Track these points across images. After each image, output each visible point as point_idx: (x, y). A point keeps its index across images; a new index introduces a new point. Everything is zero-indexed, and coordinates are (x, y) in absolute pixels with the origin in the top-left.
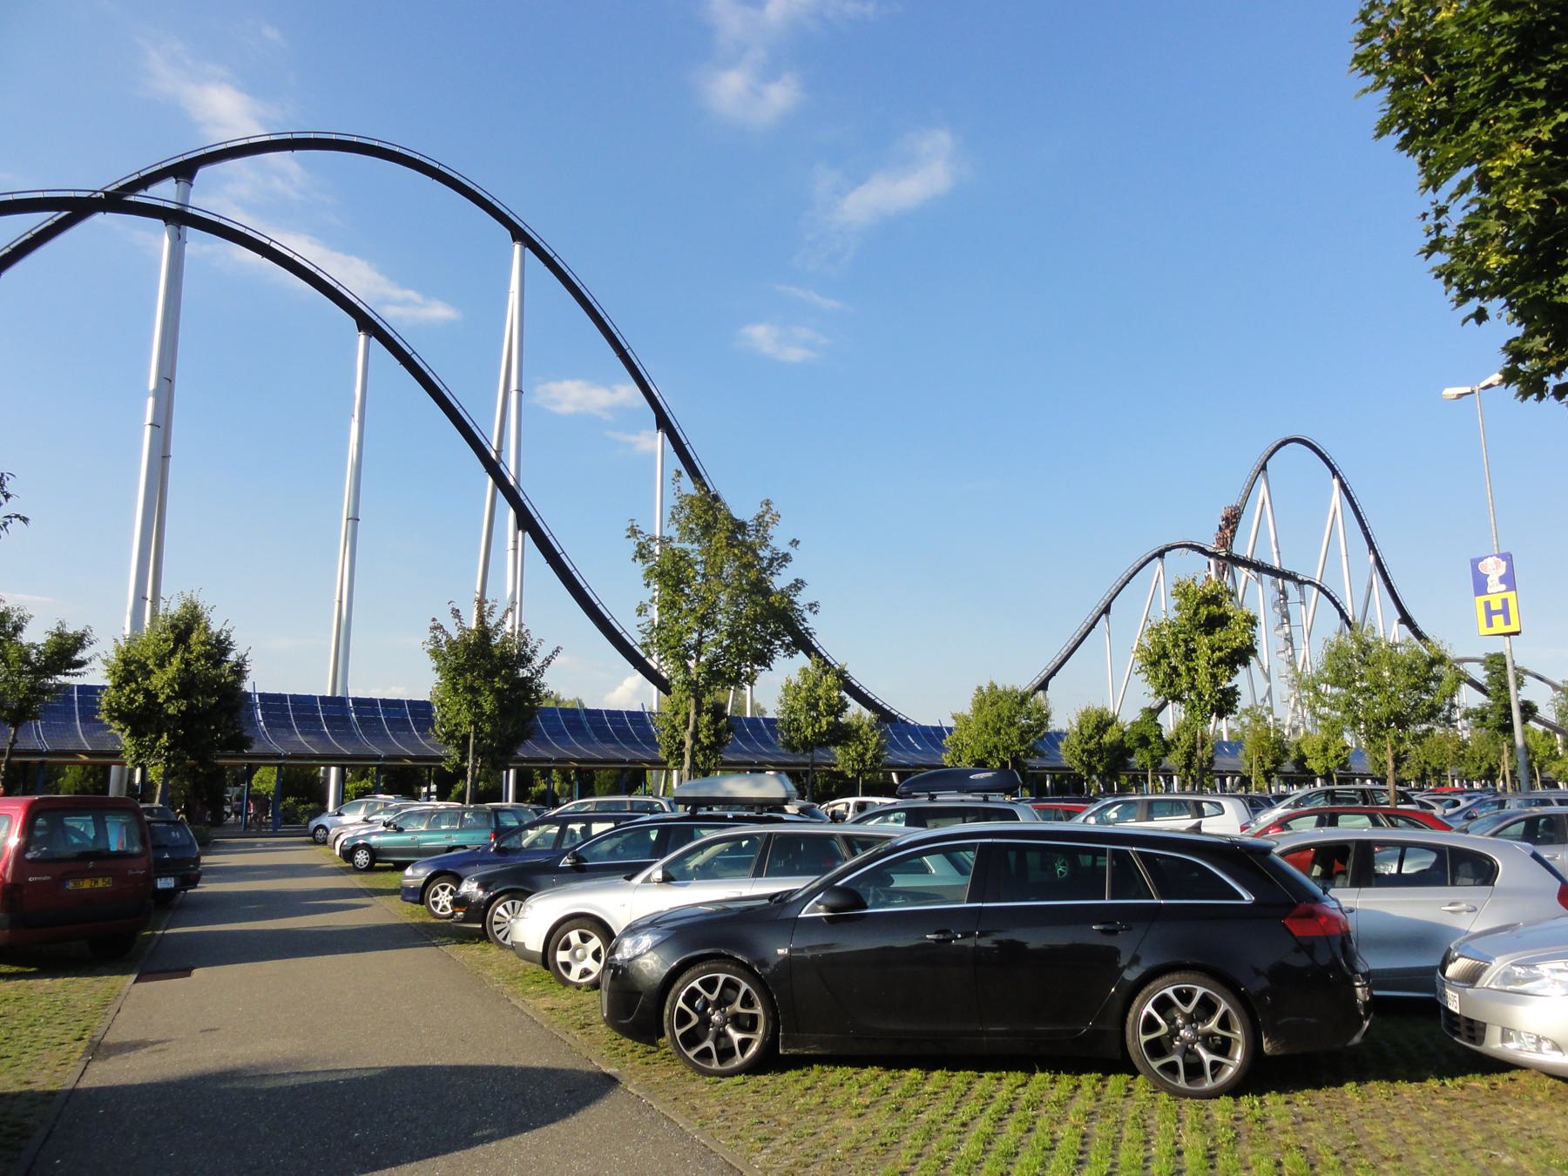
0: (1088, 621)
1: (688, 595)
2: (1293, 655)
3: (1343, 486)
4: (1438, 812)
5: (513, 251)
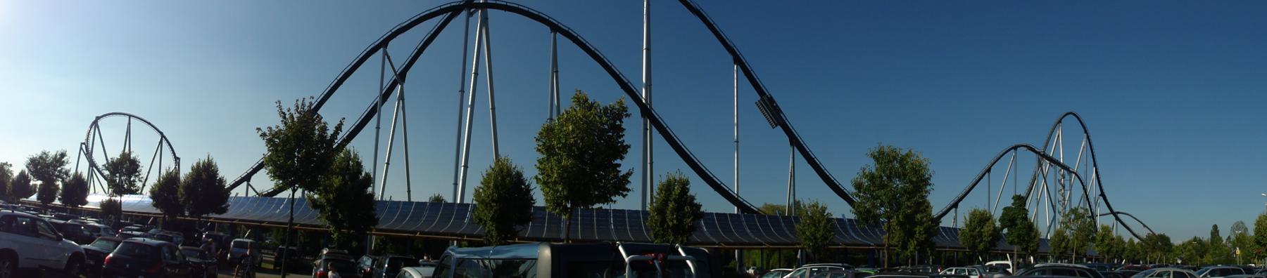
1: (830, 232)
3: (1088, 137)
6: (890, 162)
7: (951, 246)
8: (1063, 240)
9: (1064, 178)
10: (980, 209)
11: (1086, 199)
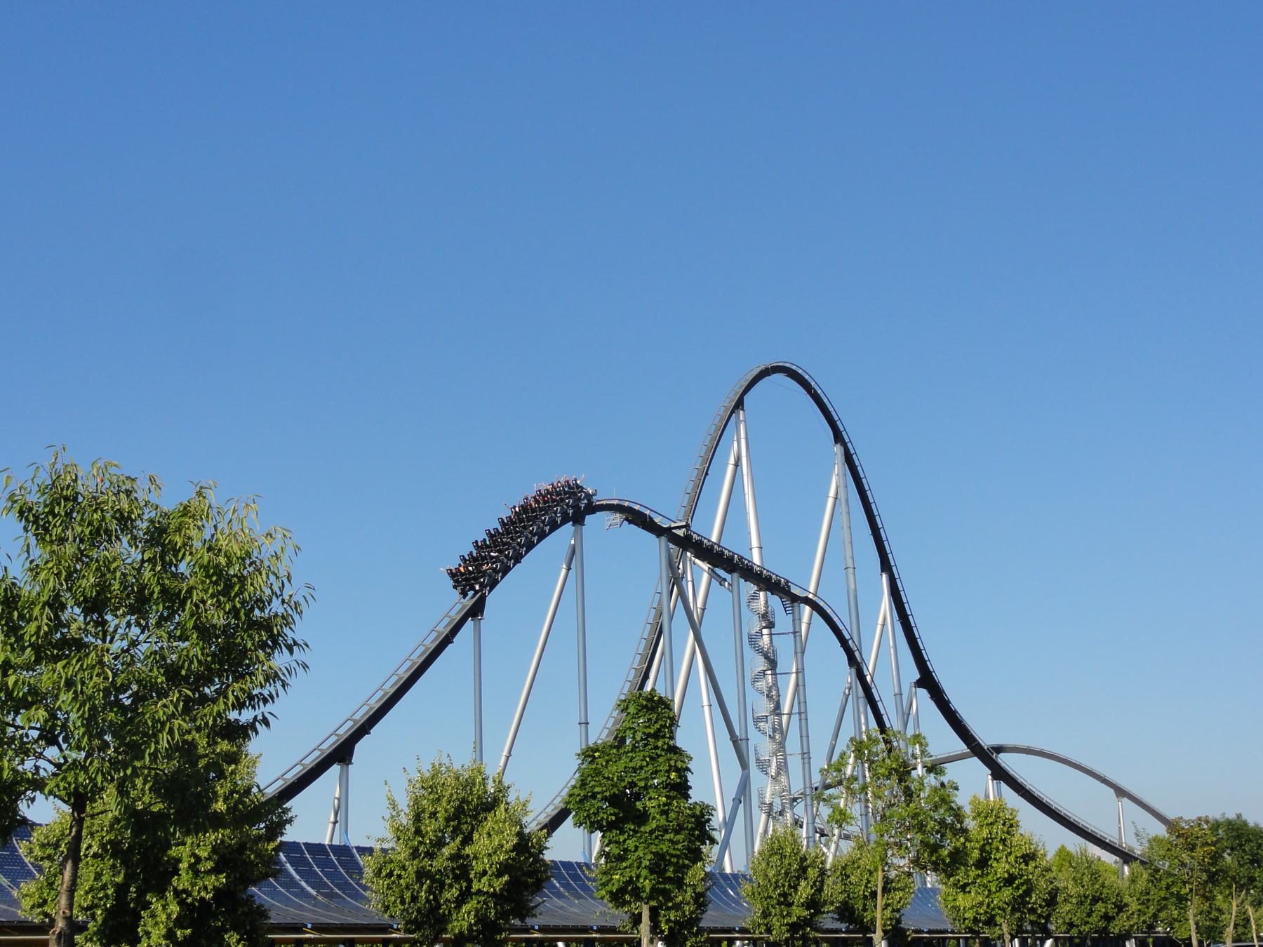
2: (775, 684)
3: (849, 459)
4: (615, 751)
6: (99, 534)
7: (932, 928)
8: (803, 870)
9: (771, 625)
10: (457, 766)
11: (862, 701)
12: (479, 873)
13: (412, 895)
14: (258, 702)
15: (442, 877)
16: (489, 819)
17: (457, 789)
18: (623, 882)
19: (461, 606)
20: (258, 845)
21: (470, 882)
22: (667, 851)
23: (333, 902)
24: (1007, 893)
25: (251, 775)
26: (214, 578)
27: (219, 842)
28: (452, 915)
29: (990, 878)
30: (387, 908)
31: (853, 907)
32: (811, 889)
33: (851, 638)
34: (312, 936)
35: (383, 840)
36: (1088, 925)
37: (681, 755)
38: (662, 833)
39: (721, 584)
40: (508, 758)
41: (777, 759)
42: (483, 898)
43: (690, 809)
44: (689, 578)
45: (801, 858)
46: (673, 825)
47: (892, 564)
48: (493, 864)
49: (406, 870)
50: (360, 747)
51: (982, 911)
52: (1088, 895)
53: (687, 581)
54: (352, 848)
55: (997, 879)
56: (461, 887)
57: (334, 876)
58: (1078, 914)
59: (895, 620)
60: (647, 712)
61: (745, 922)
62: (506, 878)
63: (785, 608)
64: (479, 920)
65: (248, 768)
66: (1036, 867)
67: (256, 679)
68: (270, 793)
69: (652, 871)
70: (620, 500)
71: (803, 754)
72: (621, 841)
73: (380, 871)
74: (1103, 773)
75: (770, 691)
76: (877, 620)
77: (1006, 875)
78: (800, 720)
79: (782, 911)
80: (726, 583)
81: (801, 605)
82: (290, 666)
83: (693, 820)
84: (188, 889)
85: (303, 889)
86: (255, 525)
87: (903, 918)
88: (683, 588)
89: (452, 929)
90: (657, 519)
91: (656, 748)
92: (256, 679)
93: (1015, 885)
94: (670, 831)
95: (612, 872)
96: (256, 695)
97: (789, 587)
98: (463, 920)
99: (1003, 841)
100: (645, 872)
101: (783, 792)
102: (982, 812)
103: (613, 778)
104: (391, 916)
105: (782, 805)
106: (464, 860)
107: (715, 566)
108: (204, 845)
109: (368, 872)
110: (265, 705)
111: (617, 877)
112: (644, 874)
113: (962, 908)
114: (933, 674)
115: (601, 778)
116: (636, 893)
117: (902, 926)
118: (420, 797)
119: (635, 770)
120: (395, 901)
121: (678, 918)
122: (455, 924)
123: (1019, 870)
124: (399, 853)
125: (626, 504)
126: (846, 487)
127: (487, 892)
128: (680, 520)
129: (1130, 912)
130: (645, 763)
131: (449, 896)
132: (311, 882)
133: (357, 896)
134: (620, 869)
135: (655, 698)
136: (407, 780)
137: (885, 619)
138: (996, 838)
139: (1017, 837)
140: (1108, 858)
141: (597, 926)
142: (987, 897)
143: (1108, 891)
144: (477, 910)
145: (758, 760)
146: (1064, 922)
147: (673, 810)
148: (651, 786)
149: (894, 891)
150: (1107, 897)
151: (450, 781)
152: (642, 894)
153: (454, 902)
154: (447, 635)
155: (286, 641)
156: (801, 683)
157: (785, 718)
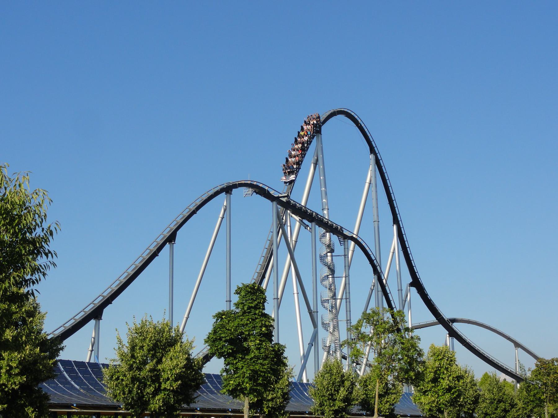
0: (151, 248)
2: (334, 282)
3: (378, 162)
5: (88, 353)
10: (155, 322)
11: (380, 293)
12: (165, 379)
13: (129, 390)
14: (30, 283)
15: (145, 381)
16: (172, 350)
17: (155, 334)
18: (235, 385)
19: (163, 236)
20: (44, 361)
21: (160, 384)
22: (259, 369)
23: (88, 393)
24: (448, 396)
25: (41, 323)
26: (4, 216)
27: (22, 358)
28: (150, 401)
29: (439, 388)
30: (116, 396)
31: (369, 402)
32: (346, 392)
33: (376, 259)
34: (76, 410)
35: (114, 360)
36: (495, 415)
37: (268, 318)
38: (256, 360)
39: (305, 228)
40: (187, 318)
41: (333, 323)
42: (167, 393)
43: (272, 347)
44: (289, 225)
45: (341, 376)
46: (263, 355)
47: (399, 220)
48: (173, 374)
49: (126, 377)
50: (106, 311)
51: (434, 405)
52: (496, 399)
53: (287, 226)
54: (100, 364)
55: (443, 389)
56: (156, 386)
57: (90, 379)
58: (490, 409)
59: (400, 250)
60: (251, 295)
61: (310, 409)
62: (180, 382)
63: (340, 242)
64: (164, 404)
65: (39, 320)
66: (463, 383)
67: (26, 271)
68: (56, 334)
69: (250, 380)
70: (252, 181)
71: (347, 320)
72: (235, 363)
73: (112, 377)
74: (508, 334)
75: (330, 286)
76: (390, 250)
77: (447, 387)
78: (346, 302)
79: (330, 403)
80: (309, 228)
81: (349, 240)
82: (46, 264)
83: (273, 353)
84: (5, 383)
85: (72, 385)
86: (28, 188)
87: (395, 408)
88: (285, 230)
89: (150, 408)
90: (272, 192)
91: (255, 314)
92: (26, 271)
93: (452, 392)
94: (261, 358)
95: (229, 380)
96: (28, 279)
97: (343, 231)
98: (156, 403)
99: (447, 369)
100: (246, 380)
101: (336, 341)
102: (436, 353)
103: (231, 329)
104: (117, 401)
105: (335, 348)
106: (158, 372)
107: (303, 218)
108: (14, 360)
109: (107, 377)
110: (33, 285)
111: (232, 382)
112: (246, 381)
113: (423, 403)
114: (419, 279)
115: (224, 329)
116: (242, 391)
117: (395, 413)
118: (135, 338)
119: (243, 325)
120: (120, 393)
121: (273, 406)
122: (152, 406)
123: (454, 384)
124: (122, 368)
125: (255, 183)
126: (376, 177)
127: (169, 389)
128: (284, 193)
129: (518, 408)
130: (249, 322)
131: (148, 391)
132: (77, 382)
133: (102, 390)
134: (233, 378)
135: (255, 288)
136: (128, 329)
137: (394, 249)
138: (443, 367)
139: (454, 366)
140: (509, 379)
141: (232, 409)
142: (437, 398)
143: (507, 397)
144: (164, 399)
145: (323, 323)
146: (483, 412)
147: (263, 347)
148: (252, 334)
149: (391, 394)
150: (506, 400)
151: (152, 330)
152: (245, 392)
153: (151, 394)
154: (155, 251)
155: (44, 250)
156: (347, 283)
157: (338, 301)
